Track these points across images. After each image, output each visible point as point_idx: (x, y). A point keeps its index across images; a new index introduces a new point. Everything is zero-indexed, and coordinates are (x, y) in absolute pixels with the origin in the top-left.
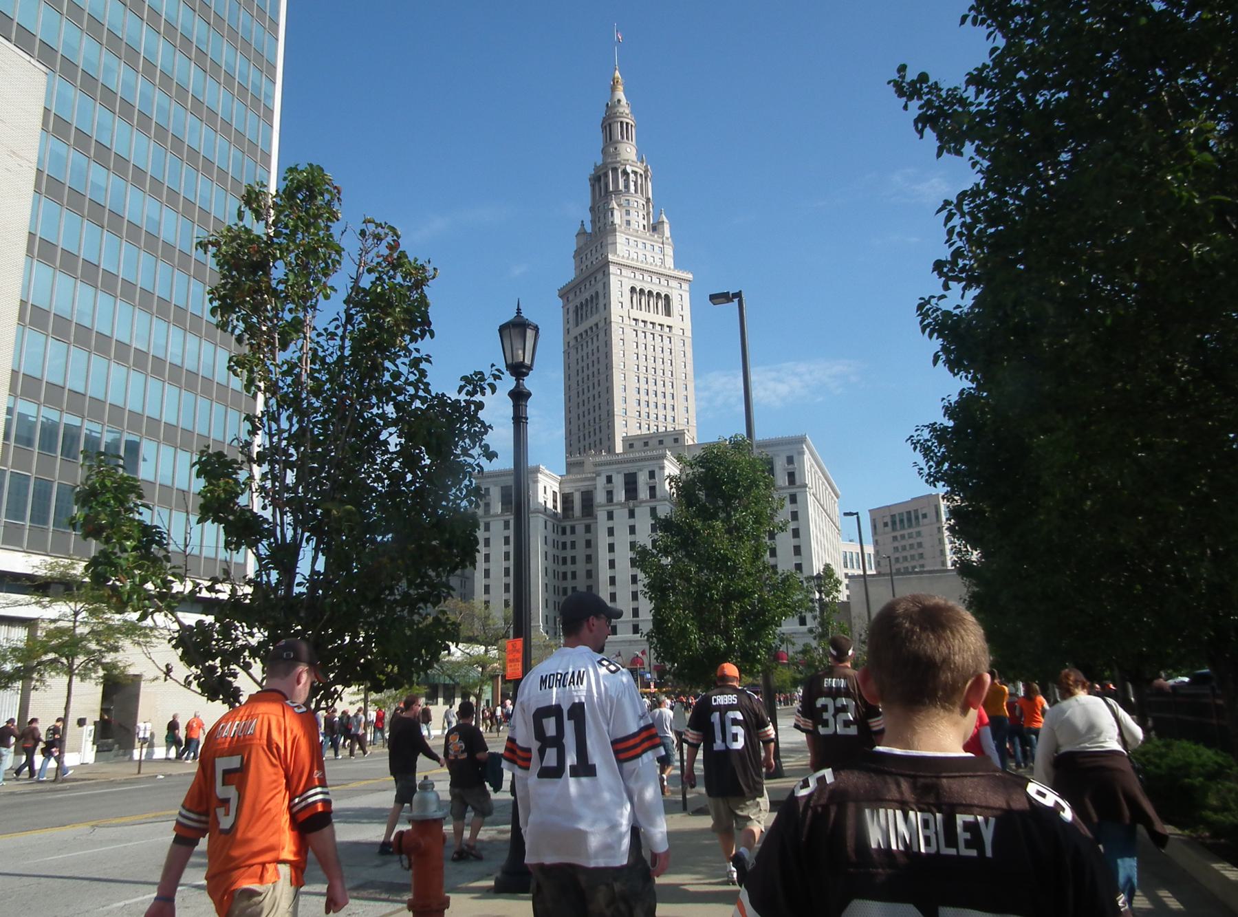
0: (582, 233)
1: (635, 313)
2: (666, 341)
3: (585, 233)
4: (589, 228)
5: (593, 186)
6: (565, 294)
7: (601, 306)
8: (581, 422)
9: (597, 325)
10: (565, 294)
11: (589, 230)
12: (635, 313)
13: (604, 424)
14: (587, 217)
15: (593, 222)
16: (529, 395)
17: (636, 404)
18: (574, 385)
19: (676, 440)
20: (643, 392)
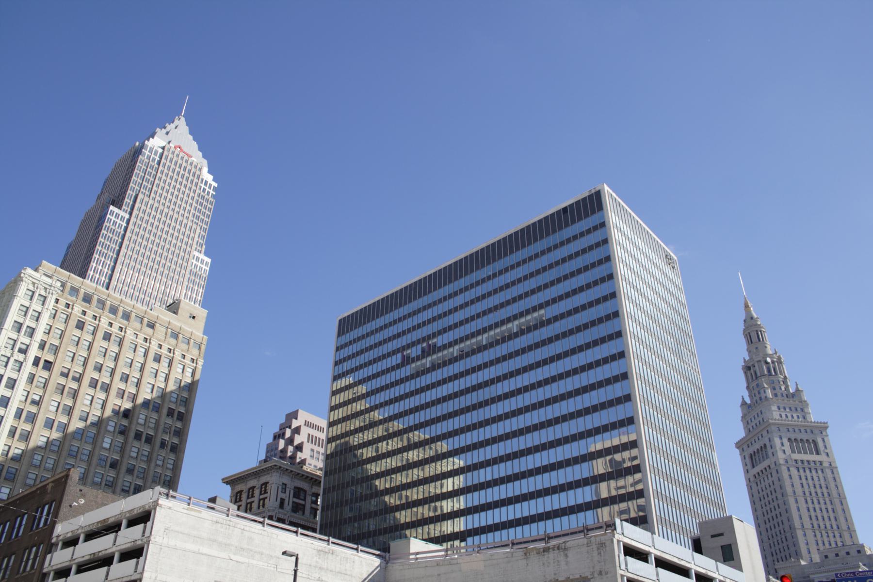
0: (744, 403)
1: (796, 456)
2: (820, 472)
3: (746, 403)
4: (748, 401)
5: (745, 373)
6: (740, 445)
7: (770, 454)
8: (763, 502)
9: (769, 466)
10: (740, 445)
11: (748, 401)
12: (796, 456)
13: (788, 535)
14: (746, 395)
15: (750, 396)
16: (822, 428)
17: (808, 519)
18: (759, 508)
19: (859, 552)
20: (812, 510)
